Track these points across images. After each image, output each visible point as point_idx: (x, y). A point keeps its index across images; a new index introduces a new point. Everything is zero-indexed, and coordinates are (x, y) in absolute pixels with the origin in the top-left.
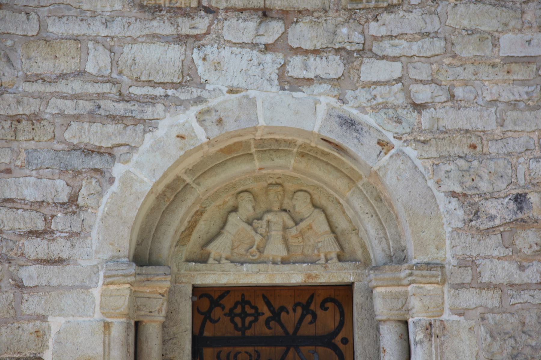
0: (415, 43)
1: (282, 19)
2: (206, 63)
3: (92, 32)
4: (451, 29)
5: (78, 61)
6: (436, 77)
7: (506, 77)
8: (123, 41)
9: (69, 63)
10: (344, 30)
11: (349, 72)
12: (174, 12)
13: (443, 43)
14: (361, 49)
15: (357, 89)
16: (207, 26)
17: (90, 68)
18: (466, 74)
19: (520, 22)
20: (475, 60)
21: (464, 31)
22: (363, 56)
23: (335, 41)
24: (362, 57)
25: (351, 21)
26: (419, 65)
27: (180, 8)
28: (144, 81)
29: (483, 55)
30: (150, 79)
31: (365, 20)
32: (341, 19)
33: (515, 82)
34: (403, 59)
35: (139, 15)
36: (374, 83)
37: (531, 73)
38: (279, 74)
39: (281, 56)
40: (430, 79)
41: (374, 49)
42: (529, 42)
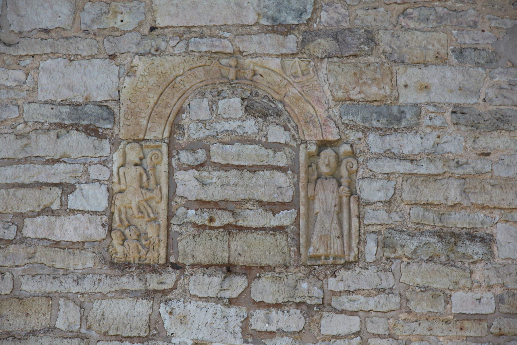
0: (371, 298)
1: (245, 274)
2: (172, 317)
3: (64, 289)
4: (405, 285)
5: (49, 317)
6: (393, 331)
7: (459, 334)
8: (93, 297)
9: (40, 319)
10: (305, 285)
11: (310, 326)
12: (143, 268)
13: (398, 299)
14: (321, 303)
15: (317, 342)
16: (174, 281)
17: (60, 324)
18: (422, 329)
19: (469, 281)
20: (429, 316)
21: (417, 288)
22: (323, 310)
23: (295, 295)
24: (322, 311)
25: (311, 276)
26: (376, 319)
27: (148, 265)
28: (111, 336)
29: (437, 311)
30: (118, 333)
31: (324, 276)
32: (300, 274)
33: (468, 339)
34: (361, 314)
35: (109, 272)
36: (334, 337)
37: (483, 330)
38: (243, 327)
39: (244, 309)
40: (387, 333)
41: (333, 304)
42: (479, 300)
